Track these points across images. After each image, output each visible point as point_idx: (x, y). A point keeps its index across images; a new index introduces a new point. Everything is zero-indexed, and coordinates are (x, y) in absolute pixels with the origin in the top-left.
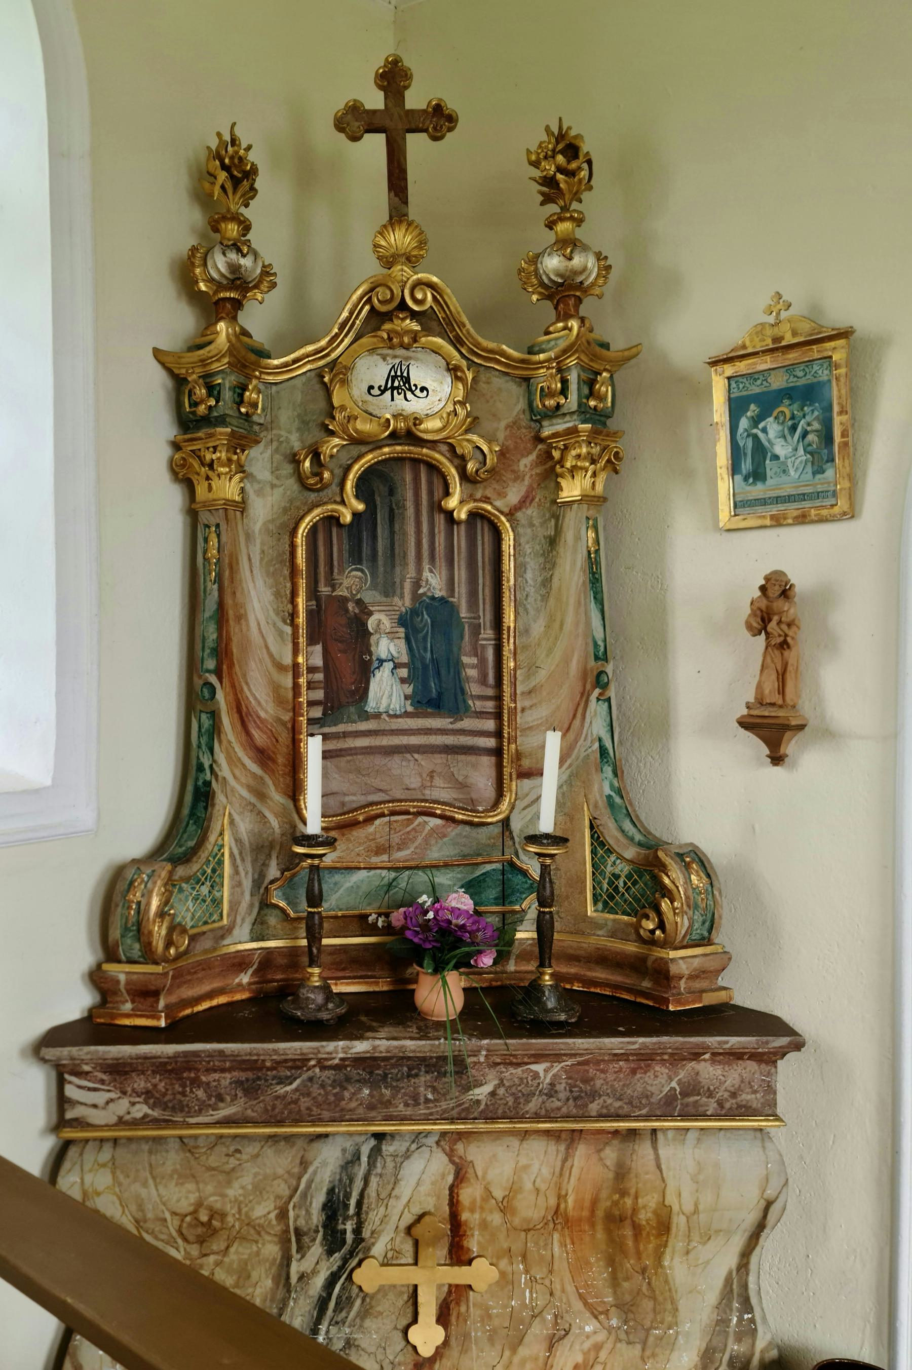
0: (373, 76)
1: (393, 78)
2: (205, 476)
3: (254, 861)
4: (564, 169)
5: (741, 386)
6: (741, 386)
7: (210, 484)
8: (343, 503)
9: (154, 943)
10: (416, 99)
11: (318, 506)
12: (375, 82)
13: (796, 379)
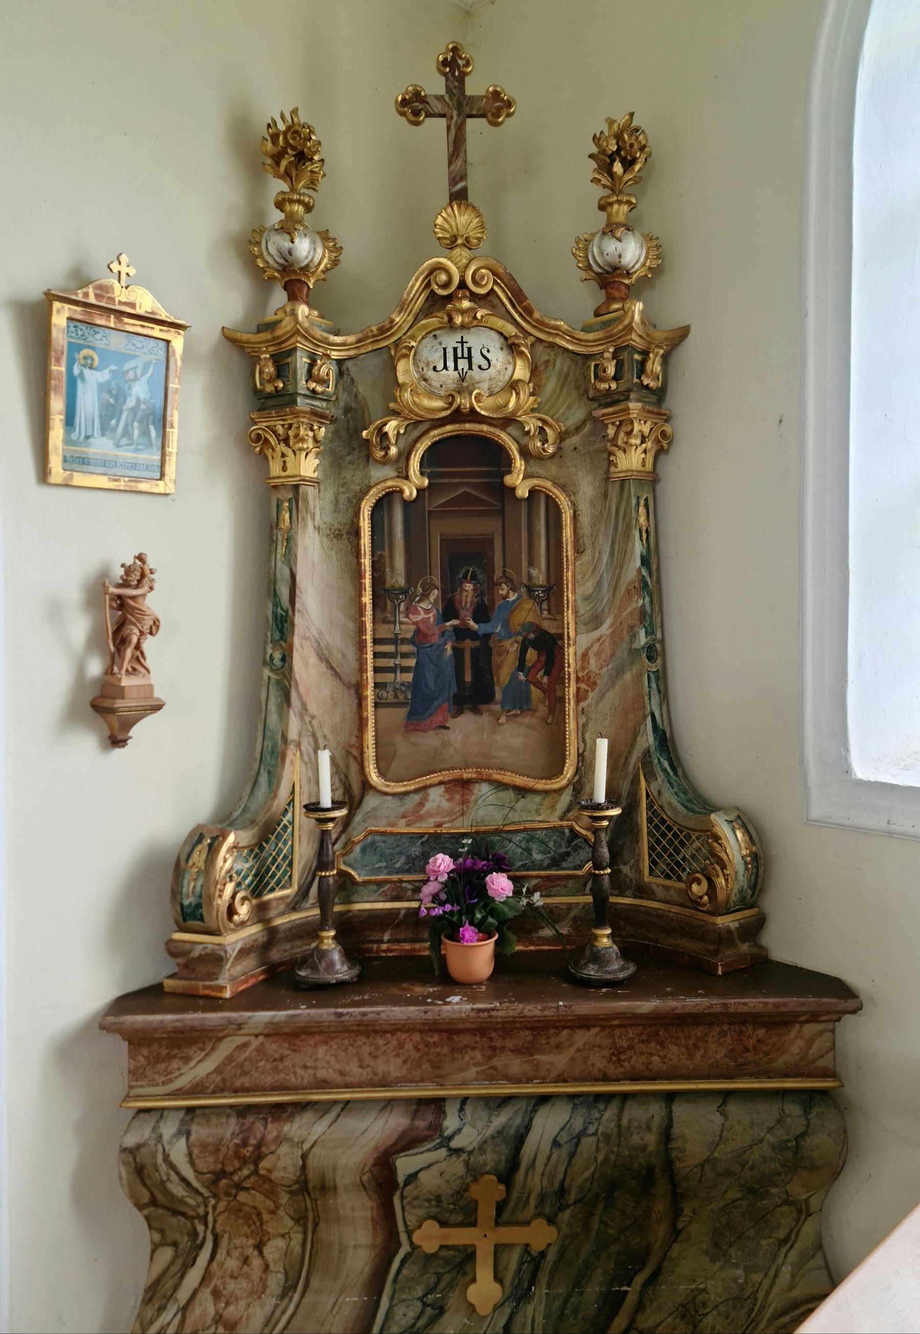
0: (435, 65)
1: (453, 66)
2: (280, 454)
3: (610, 326)
4: (621, 156)
5: (80, 333)
6: (80, 333)
7: (284, 462)
8: (407, 478)
9: (523, 463)
10: (475, 86)
11: (361, 499)
12: (438, 68)
13: (133, 348)
